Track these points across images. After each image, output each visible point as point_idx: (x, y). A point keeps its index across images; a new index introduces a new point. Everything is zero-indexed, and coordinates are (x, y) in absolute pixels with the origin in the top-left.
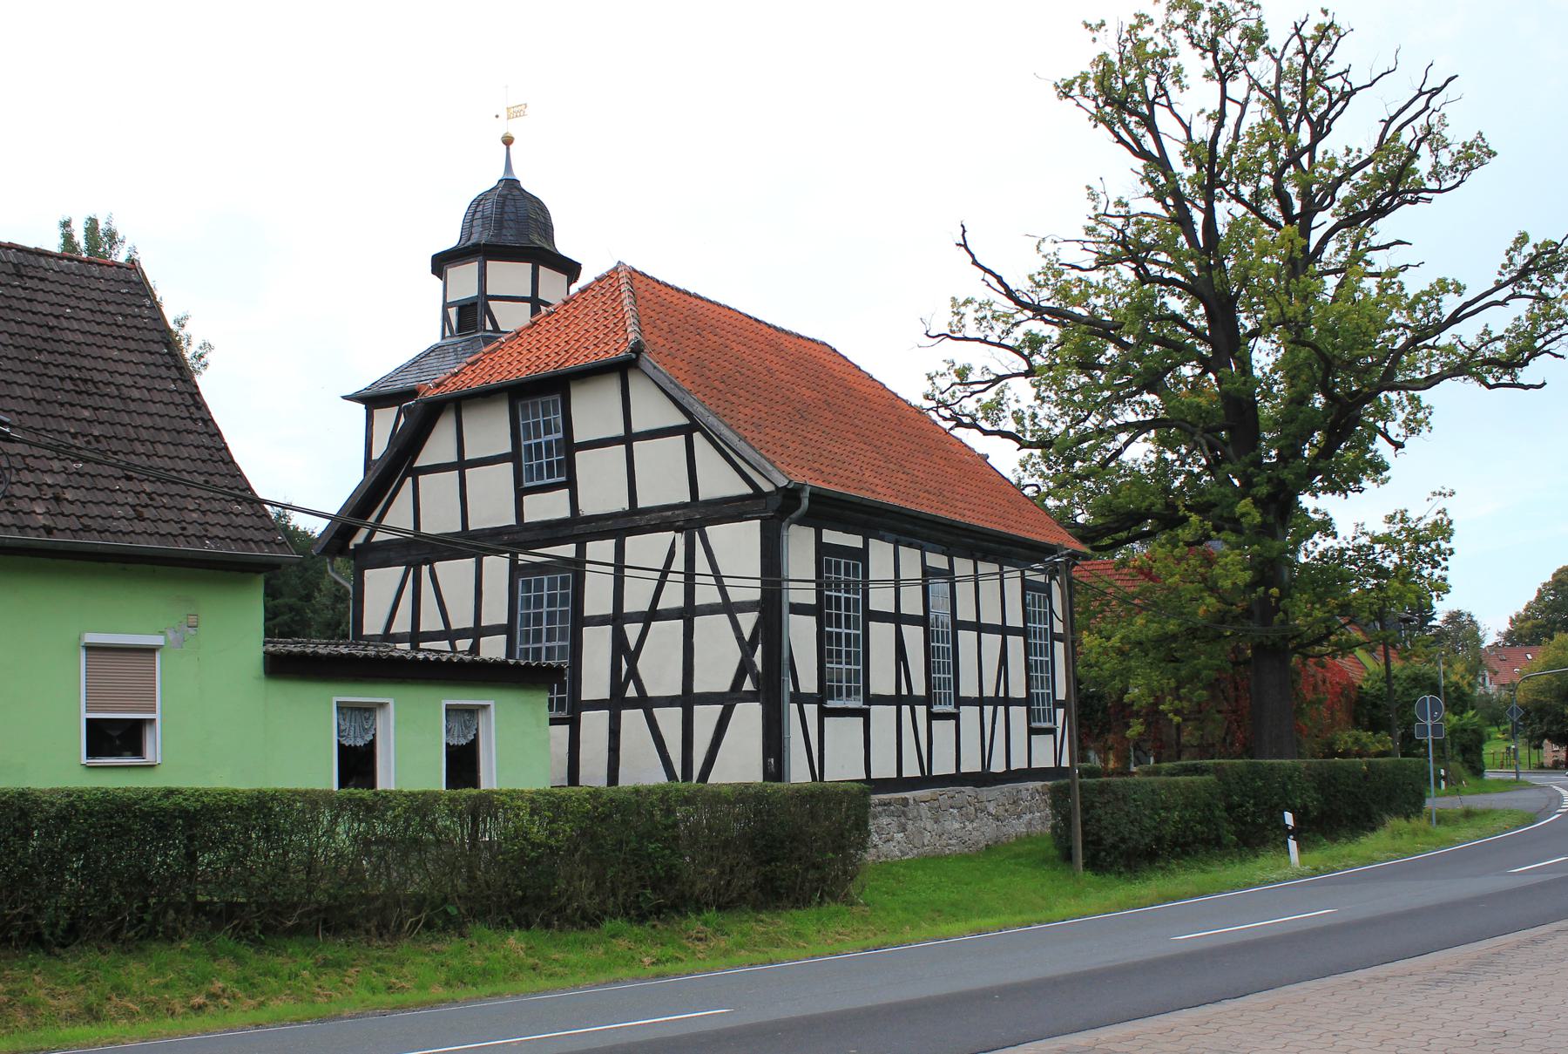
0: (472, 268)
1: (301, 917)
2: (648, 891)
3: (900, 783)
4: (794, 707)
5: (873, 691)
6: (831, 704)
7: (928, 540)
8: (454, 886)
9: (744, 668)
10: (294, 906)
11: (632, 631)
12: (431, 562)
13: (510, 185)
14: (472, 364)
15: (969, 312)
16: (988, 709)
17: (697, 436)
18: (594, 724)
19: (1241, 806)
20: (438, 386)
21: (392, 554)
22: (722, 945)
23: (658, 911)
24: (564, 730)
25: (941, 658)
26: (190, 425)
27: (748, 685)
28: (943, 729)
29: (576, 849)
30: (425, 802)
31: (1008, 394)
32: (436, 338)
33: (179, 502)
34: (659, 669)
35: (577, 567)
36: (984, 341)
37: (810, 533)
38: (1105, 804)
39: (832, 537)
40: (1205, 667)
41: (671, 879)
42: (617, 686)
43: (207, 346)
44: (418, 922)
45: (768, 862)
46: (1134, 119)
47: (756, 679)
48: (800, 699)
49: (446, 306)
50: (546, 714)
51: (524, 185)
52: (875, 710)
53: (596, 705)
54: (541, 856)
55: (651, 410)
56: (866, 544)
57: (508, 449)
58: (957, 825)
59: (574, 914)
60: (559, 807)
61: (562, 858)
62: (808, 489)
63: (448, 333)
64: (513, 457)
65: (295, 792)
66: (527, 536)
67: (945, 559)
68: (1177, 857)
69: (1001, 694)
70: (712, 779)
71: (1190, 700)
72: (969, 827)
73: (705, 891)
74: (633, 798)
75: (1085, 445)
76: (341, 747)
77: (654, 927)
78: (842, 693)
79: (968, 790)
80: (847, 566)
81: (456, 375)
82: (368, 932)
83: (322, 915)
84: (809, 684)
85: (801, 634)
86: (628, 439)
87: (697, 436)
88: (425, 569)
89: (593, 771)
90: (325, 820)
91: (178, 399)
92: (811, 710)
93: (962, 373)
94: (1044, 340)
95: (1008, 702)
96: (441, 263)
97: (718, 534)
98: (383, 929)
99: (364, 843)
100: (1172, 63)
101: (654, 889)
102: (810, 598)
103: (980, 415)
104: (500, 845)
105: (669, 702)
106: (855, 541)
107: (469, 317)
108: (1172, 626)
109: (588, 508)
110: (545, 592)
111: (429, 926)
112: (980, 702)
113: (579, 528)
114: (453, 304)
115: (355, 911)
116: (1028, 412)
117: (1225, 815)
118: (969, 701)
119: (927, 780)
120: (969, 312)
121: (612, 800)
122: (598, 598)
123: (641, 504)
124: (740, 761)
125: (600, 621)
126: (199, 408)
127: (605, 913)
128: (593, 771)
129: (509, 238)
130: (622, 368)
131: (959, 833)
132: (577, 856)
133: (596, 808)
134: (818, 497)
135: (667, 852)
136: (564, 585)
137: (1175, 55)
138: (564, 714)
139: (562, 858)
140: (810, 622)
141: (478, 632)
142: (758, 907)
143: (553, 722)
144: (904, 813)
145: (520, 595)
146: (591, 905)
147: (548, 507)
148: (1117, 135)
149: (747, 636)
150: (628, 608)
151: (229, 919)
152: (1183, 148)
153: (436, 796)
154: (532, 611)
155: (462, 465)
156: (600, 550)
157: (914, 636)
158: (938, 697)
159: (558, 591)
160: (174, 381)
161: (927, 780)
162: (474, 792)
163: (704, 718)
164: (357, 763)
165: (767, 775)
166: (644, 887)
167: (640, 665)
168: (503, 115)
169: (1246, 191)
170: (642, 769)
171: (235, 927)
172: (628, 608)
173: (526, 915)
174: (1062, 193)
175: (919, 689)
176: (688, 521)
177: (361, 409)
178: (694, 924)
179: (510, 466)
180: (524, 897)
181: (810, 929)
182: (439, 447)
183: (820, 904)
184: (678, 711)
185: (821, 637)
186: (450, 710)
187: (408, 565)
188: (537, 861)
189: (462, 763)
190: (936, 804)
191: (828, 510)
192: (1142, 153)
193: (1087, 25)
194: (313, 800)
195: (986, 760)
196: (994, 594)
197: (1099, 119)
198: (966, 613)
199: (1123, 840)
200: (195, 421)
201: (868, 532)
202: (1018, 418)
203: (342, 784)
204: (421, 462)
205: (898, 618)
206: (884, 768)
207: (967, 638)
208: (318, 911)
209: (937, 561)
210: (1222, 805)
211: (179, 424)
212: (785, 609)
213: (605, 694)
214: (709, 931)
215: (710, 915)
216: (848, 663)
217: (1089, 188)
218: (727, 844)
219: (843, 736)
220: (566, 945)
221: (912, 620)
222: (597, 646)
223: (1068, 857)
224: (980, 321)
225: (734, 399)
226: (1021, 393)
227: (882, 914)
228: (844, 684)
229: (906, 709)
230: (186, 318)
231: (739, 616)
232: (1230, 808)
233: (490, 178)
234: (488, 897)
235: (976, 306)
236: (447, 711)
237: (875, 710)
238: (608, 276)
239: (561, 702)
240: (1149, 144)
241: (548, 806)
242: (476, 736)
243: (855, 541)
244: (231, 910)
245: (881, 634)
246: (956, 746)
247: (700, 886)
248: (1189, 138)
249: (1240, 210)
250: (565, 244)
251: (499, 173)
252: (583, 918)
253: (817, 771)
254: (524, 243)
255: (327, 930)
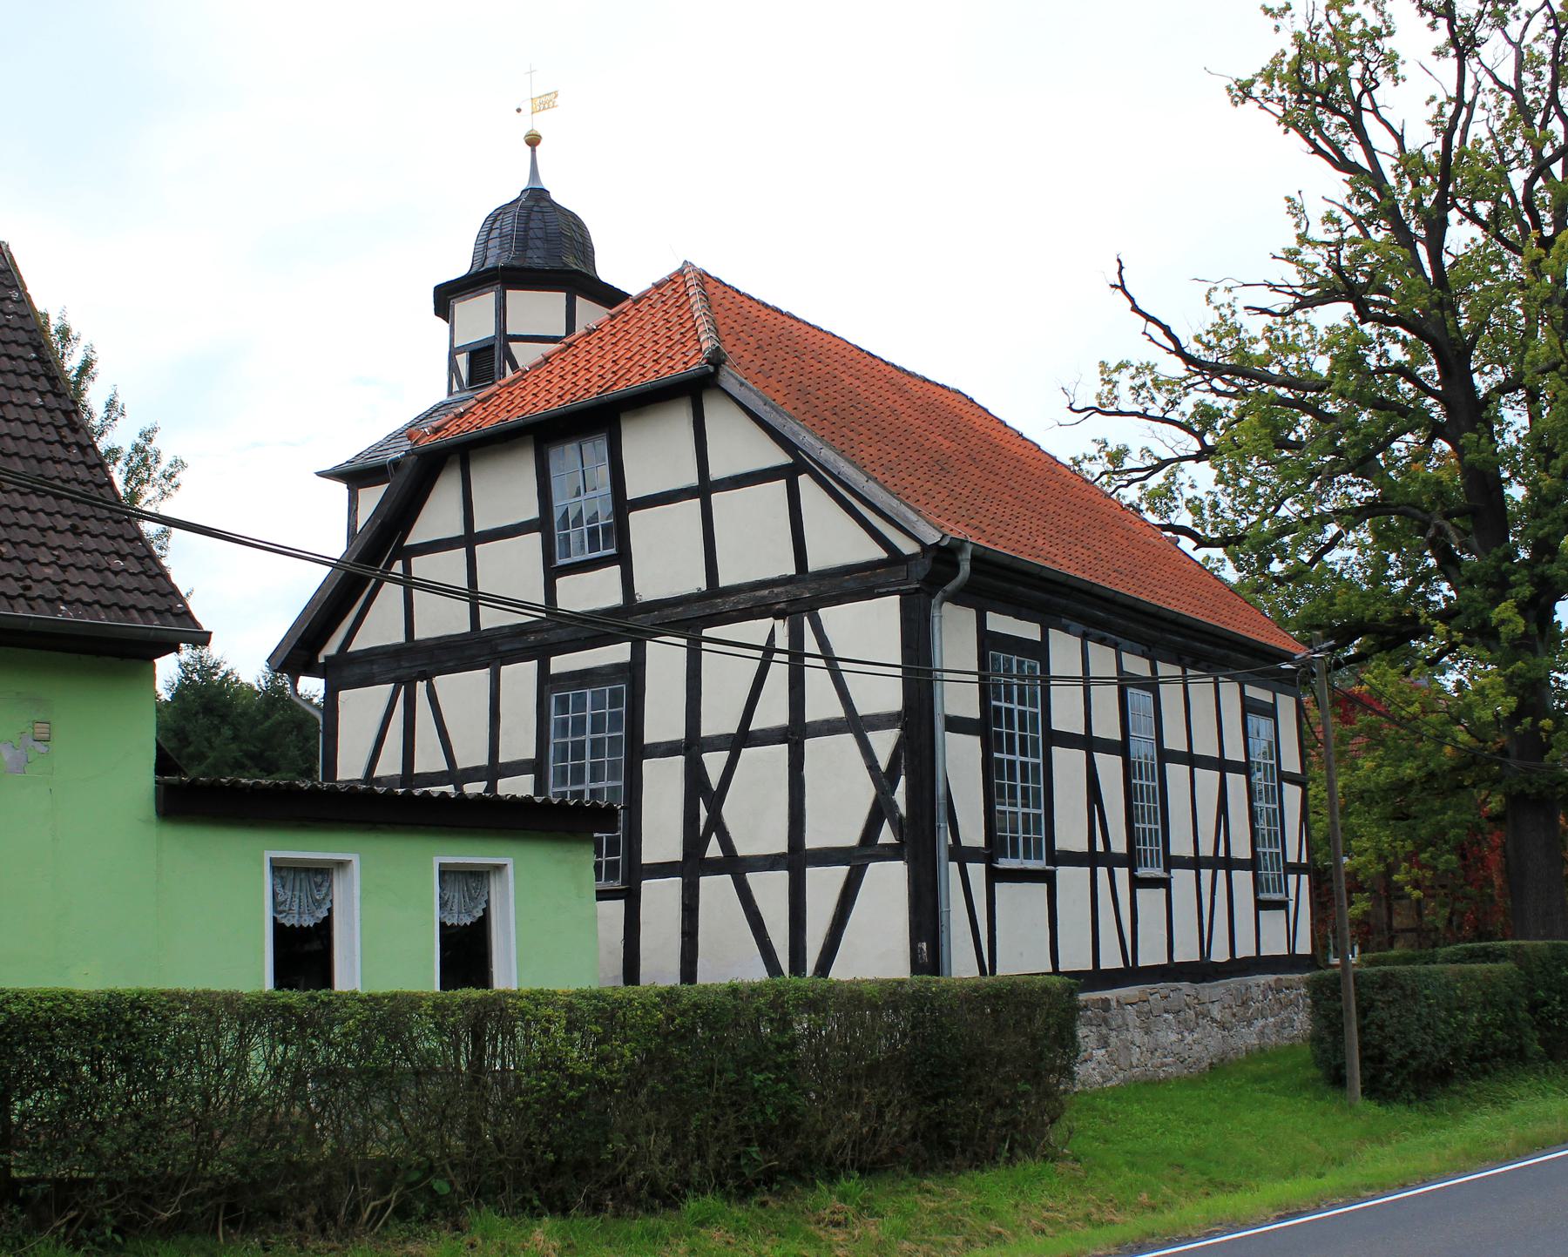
0: (488, 300)
1: (185, 1203)
2: (754, 1150)
3: (1097, 978)
4: (954, 866)
5: (1058, 846)
6: (1005, 863)
7: (1124, 634)
8: (444, 1146)
9: (880, 811)
10: (171, 1185)
11: (714, 763)
12: (427, 677)
13: (536, 197)
14: (484, 401)
15: (1124, 380)
16: (1206, 874)
17: (804, 481)
18: (661, 900)
19: (1545, 1004)
20: (436, 430)
21: (376, 668)
22: (873, 1232)
23: (769, 1178)
24: (618, 906)
25: (1147, 802)
26: (58, 451)
27: (886, 836)
28: (1150, 900)
29: (641, 1083)
30: (395, 1013)
31: (1181, 477)
32: (442, 396)
33: (27, 552)
34: (755, 820)
35: (633, 673)
36: (1143, 415)
37: (970, 614)
38: (1389, 1003)
39: (999, 623)
40: (1454, 825)
41: (790, 1128)
42: (693, 841)
43: (179, 464)
44: (387, 1204)
45: (934, 1099)
46: (1338, 119)
47: (898, 826)
48: (962, 855)
49: (453, 352)
50: (591, 884)
51: (556, 197)
52: (1062, 872)
53: (662, 870)
54: (584, 1097)
55: (737, 445)
56: (1045, 635)
57: (533, 513)
58: (1173, 1037)
59: (639, 1189)
60: (613, 1016)
61: (619, 1098)
62: (970, 548)
63: (456, 388)
64: (543, 524)
65: (178, 997)
66: (562, 634)
67: (1146, 663)
68: (1475, 1077)
69: (1222, 853)
70: (837, 973)
71: (1435, 868)
72: (1189, 1038)
73: (841, 1146)
74: (730, 1002)
75: (1287, 539)
76: (278, 928)
77: (763, 1204)
78: (1018, 849)
79: (1185, 986)
80: (1020, 664)
81: (461, 415)
82: (301, 1225)
83: (222, 1200)
84: (973, 833)
85: (961, 760)
86: (704, 489)
87: (804, 481)
88: (421, 687)
89: (660, 963)
90: (228, 1042)
91: (44, 417)
92: (977, 871)
93: (1117, 457)
94: (1218, 414)
95: (1229, 864)
96: (446, 298)
97: (835, 618)
98: (326, 1220)
99: (290, 1076)
100: (1386, 44)
101: (762, 1145)
102: (807, 661)
103: (1144, 506)
104: (518, 1079)
105: (769, 863)
106: (1029, 631)
107: (482, 363)
108: (1408, 770)
109: (646, 591)
110: (589, 712)
111: (403, 1212)
112: (1196, 863)
113: (635, 621)
114: (461, 350)
115: (278, 1192)
116: (1208, 500)
117: (1528, 1016)
118: (1182, 863)
119: (1132, 974)
120: (1124, 380)
121: (696, 1006)
122: (663, 718)
123: (724, 582)
124: (876, 948)
125: (668, 749)
126: (75, 431)
127: (687, 1185)
128: (660, 963)
129: (536, 259)
130: (694, 390)
131: (1176, 1048)
132: (642, 1098)
133: (671, 1019)
134: (984, 562)
135: (784, 1086)
136: (615, 699)
137: (1390, 34)
138: (617, 885)
139: (619, 1098)
140: (974, 743)
141: (494, 770)
142: (920, 1168)
143: (602, 895)
144: (1106, 1021)
145: (553, 717)
146: (665, 1173)
147: (590, 592)
148: (1312, 143)
149: (883, 764)
150: (707, 730)
151: (61, 1209)
152: (1395, 162)
153: (414, 1001)
154: (569, 739)
155: (470, 540)
156: (665, 660)
157: (1110, 767)
158: (1142, 858)
159: (607, 710)
160: (42, 394)
161: (1132, 974)
162: (475, 993)
163: (824, 884)
164: (303, 952)
165: (916, 967)
166: (748, 1142)
167: (727, 811)
168: (527, 108)
169: (1483, 209)
170: (730, 960)
171: (72, 1222)
172: (707, 730)
173: (561, 1191)
174: (1243, 224)
175: (1119, 845)
176: (791, 602)
177: (341, 489)
178: (826, 1199)
179: (536, 538)
180: (558, 1162)
181: (1004, 1204)
182: (439, 516)
183: (1009, 1161)
184: (783, 869)
185: (990, 768)
186: (446, 873)
187: (398, 682)
188: (580, 1104)
189: (465, 952)
190: (1146, 1007)
191: (999, 583)
192: (1343, 164)
193: (1267, 11)
194: (213, 1009)
195: (1205, 945)
196: (1203, 711)
197: (1288, 121)
198: (1174, 740)
199: (1413, 1054)
200: (67, 446)
201: (1049, 617)
202: (1195, 507)
203: (281, 980)
204: (414, 539)
205: (1088, 743)
206: (1075, 957)
207: (1177, 774)
208: (213, 1193)
209: (1137, 665)
210: (1524, 1003)
211: (42, 450)
212: (939, 724)
213: (675, 853)
214: (850, 1209)
215: (850, 1184)
216: (1025, 805)
217: (1288, 199)
218: (873, 1069)
219: (1020, 907)
220: (628, 1239)
221: (1108, 747)
222: (663, 785)
223: (1338, 1079)
224: (1136, 390)
225: (852, 435)
226: (1201, 479)
227: (1102, 1174)
228: (1021, 835)
229: (1102, 872)
230: (155, 430)
231: (872, 736)
232: (1534, 1007)
233: (510, 188)
234: (500, 1164)
235: (1132, 371)
236: (442, 873)
237: (1062, 872)
238: (671, 280)
239: (613, 867)
240: (1356, 154)
241: (597, 1016)
242: (486, 911)
243: (1029, 631)
244: (65, 1193)
245: (1069, 763)
246: (1168, 925)
247: (833, 1139)
248: (1402, 148)
249: (1476, 231)
250: (608, 270)
251: (524, 183)
252: (653, 1194)
253: (987, 961)
254: (557, 265)
255: (233, 1223)
